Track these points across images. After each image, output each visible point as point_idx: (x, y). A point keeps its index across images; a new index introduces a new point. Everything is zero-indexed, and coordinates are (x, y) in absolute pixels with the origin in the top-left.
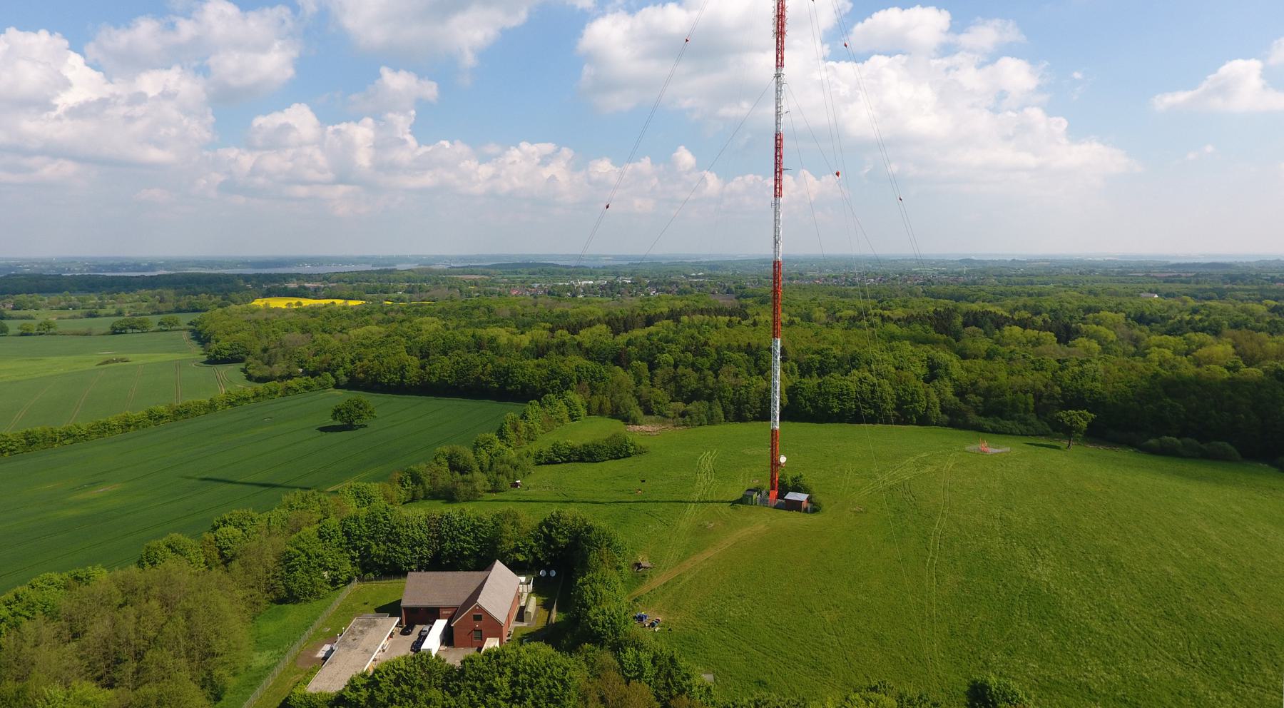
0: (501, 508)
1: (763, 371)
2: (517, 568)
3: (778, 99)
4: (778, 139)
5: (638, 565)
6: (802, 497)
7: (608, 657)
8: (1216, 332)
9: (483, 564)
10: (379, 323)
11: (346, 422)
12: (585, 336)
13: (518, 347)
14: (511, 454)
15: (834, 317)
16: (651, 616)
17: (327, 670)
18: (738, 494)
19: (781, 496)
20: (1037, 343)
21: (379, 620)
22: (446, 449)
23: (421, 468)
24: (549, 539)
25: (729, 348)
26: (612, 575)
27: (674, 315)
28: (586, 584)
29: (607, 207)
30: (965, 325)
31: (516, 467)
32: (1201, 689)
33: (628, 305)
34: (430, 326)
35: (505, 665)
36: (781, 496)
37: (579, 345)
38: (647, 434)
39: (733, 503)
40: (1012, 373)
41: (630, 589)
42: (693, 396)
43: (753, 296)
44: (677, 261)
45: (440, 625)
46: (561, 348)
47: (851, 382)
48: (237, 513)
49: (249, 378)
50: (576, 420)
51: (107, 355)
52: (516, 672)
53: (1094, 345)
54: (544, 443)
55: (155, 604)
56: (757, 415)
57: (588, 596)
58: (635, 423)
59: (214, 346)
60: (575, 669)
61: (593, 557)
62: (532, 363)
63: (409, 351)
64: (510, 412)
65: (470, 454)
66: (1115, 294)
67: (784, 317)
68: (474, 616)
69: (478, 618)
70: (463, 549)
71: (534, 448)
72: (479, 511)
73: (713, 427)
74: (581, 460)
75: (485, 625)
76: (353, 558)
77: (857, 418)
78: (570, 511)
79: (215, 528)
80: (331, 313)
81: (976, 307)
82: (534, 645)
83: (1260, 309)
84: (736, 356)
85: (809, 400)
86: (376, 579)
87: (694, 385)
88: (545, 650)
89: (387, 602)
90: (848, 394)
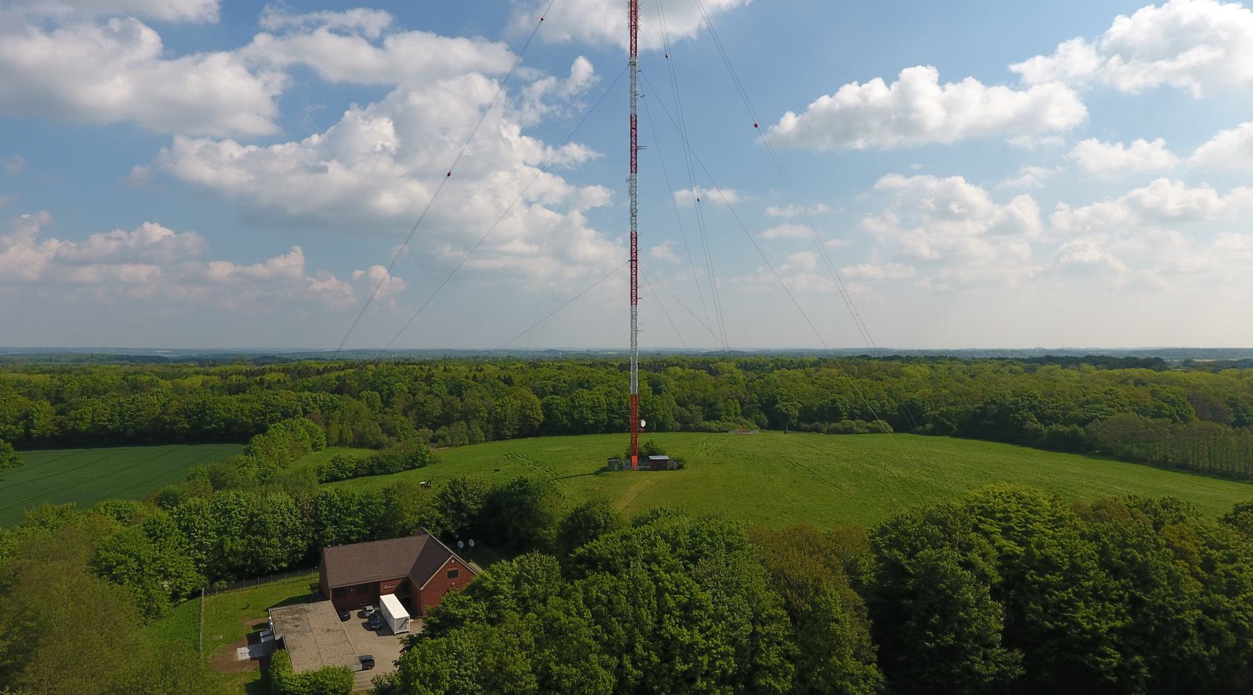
24: (459, 507)
29: (449, 175)
42: (446, 420)
44: (256, 357)
50: (318, 450)
56: (515, 432)
68: (448, 572)
70: (351, 532)
74: (372, 473)
76: (198, 561)
85: (565, 413)
86: (233, 587)
87: (438, 412)
90: (600, 406)
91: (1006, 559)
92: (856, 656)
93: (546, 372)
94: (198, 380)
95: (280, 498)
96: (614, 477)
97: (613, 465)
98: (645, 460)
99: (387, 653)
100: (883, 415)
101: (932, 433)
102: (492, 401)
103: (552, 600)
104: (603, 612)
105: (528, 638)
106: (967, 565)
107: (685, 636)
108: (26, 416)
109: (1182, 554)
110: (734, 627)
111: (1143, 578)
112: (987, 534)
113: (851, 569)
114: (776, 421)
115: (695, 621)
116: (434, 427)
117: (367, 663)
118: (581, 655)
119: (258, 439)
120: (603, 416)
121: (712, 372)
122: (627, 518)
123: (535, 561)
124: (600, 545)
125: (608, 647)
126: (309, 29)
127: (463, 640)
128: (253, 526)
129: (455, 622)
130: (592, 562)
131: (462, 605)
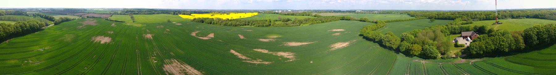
24: (476, 28)
42: (475, 18)
87: (473, 17)
91: (537, 32)
92: (522, 43)
93: (486, 13)
94: (449, 13)
95: (457, 26)
96: (494, 25)
97: (494, 24)
98: (498, 23)
99: (468, 44)
100: (525, 16)
101: (530, 18)
102: (479, 16)
103: (487, 39)
104: (493, 41)
105: (484, 43)
106: (533, 33)
107: (503, 43)
108: (436, 16)
109: (552, 29)
110: (508, 42)
111: (549, 31)
112: (535, 29)
113: (521, 35)
114: (513, 17)
115: (504, 42)
116: (473, 19)
117: (466, 44)
118: (490, 45)
119: (455, 20)
120: (493, 18)
121: (506, 12)
122: (496, 30)
123: (485, 35)
124: (493, 33)
125: (494, 44)
126: (512, 17)
127: (477, 43)
128: (454, 29)
129: (476, 41)
130: (491, 35)
131: (477, 39)
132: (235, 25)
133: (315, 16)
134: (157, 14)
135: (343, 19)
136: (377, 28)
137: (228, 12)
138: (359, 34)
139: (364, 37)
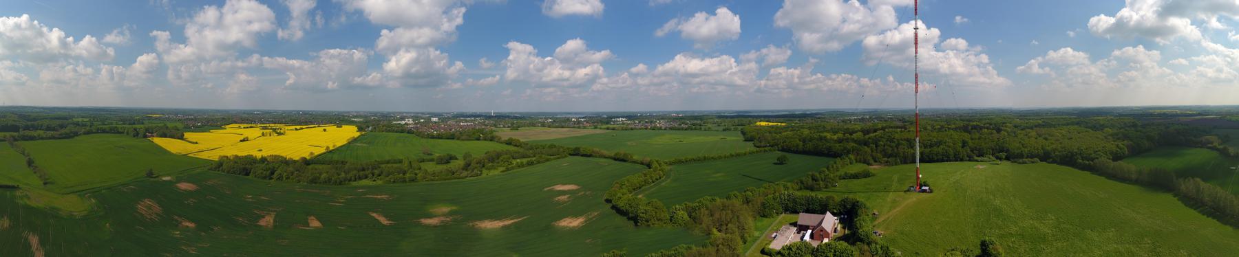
0: (829, 194)
1: (912, 146)
2: (834, 214)
3: (916, 63)
4: (916, 75)
5: (874, 214)
6: (927, 188)
7: (866, 247)
8: (1032, 128)
9: (823, 213)
10: (791, 131)
11: (781, 162)
12: (854, 136)
13: (833, 140)
14: (832, 175)
15: (933, 129)
16: (879, 232)
17: (775, 241)
18: (906, 189)
19: (920, 188)
20: (992, 133)
21: (791, 228)
22: (810, 173)
23: (804, 179)
25: (901, 140)
26: (866, 217)
27: (883, 129)
28: (858, 221)
30: (972, 129)
31: (833, 180)
32: (1037, 225)
33: (869, 125)
34: (806, 132)
35: (832, 249)
36: (920, 188)
37: (853, 139)
38: (874, 169)
39: (905, 191)
40: (986, 143)
41: (872, 223)
43: (908, 121)
45: (809, 232)
46: (847, 140)
47: (940, 149)
48: (751, 187)
49: (755, 146)
51: (722, 137)
52: (835, 251)
53: (1006, 134)
54: (842, 172)
55: (730, 212)
57: (858, 225)
58: (871, 165)
59: (746, 136)
60: (854, 251)
61: (860, 211)
62: (837, 145)
63: (800, 140)
64: (831, 161)
65: (818, 176)
66: (1010, 118)
67: (919, 129)
69: (822, 231)
71: (838, 173)
72: (821, 195)
73: (897, 167)
74: (854, 178)
75: (824, 233)
77: (942, 161)
78: (851, 196)
79: (745, 192)
80: (777, 127)
81: (975, 123)
82: (841, 242)
83: (1040, 122)
84: (903, 142)
87: (890, 152)
88: (845, 244)
89: (793, 221)
132: (338, 181)
133: (507, 144)
134: (85, 134)
135: (576, 153)
136: (643, 183)
137: (273, 120)
138: (606, 197)
139: (614, 207)
